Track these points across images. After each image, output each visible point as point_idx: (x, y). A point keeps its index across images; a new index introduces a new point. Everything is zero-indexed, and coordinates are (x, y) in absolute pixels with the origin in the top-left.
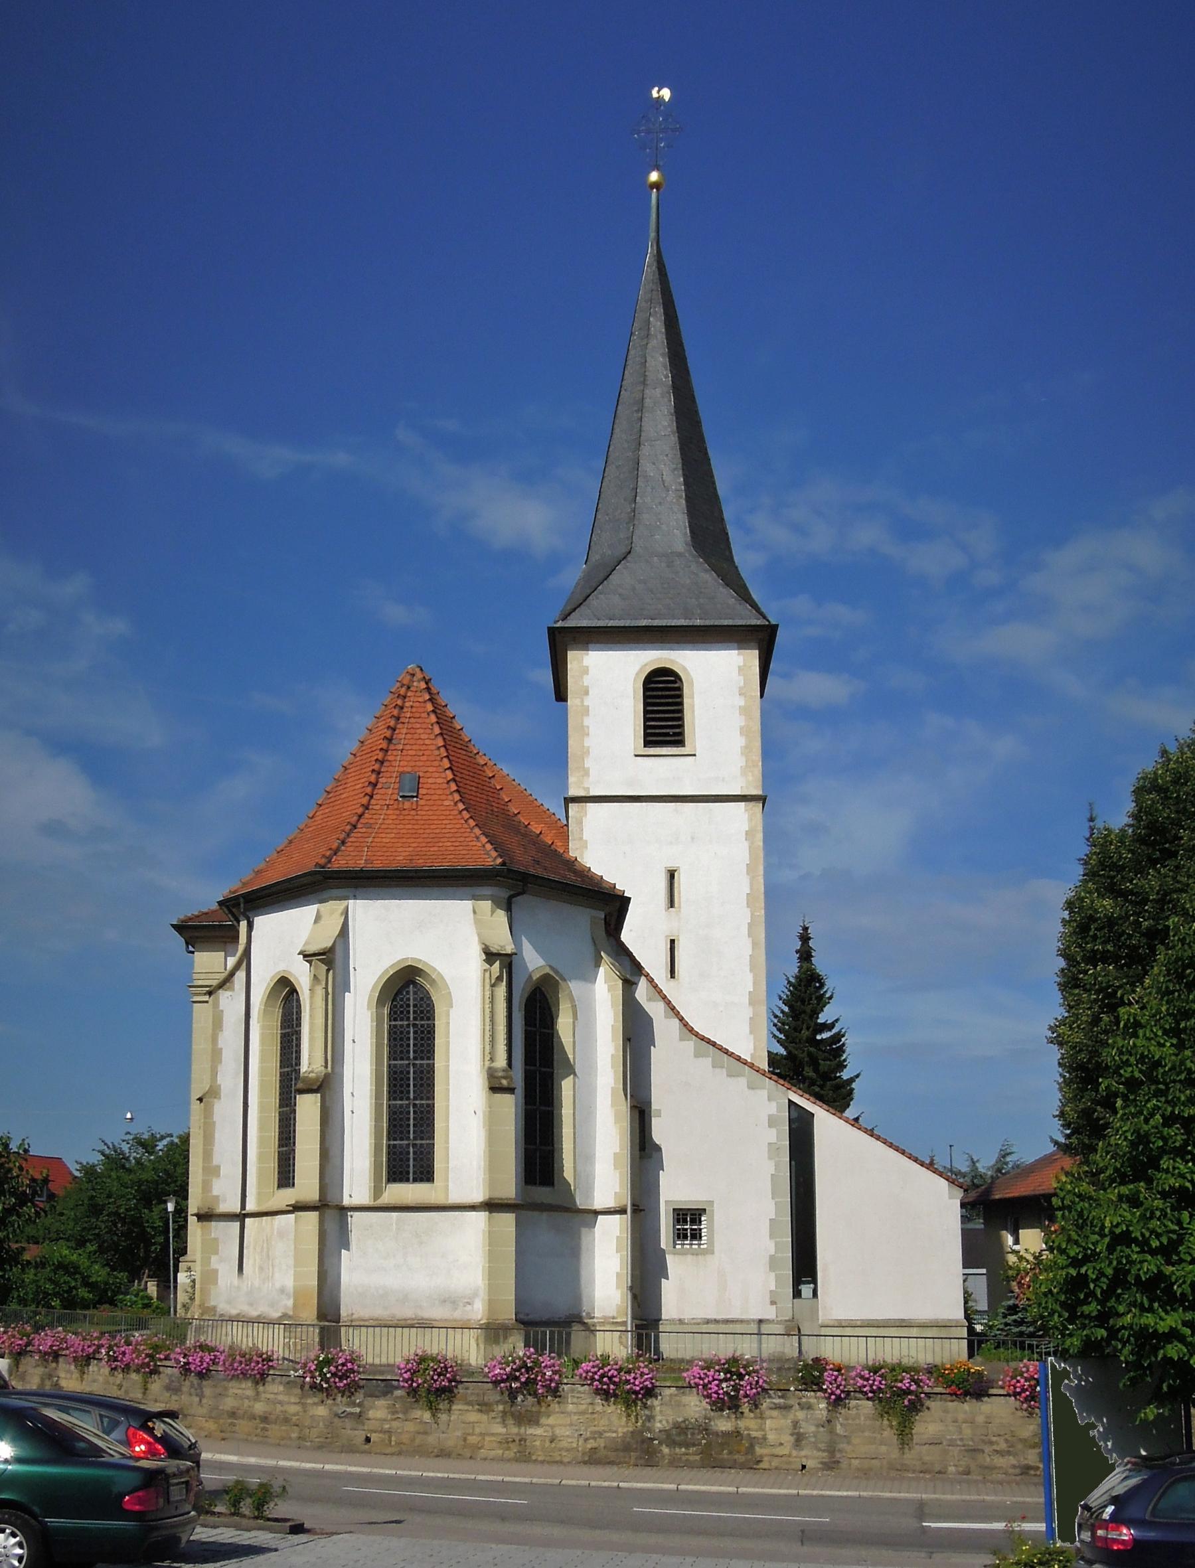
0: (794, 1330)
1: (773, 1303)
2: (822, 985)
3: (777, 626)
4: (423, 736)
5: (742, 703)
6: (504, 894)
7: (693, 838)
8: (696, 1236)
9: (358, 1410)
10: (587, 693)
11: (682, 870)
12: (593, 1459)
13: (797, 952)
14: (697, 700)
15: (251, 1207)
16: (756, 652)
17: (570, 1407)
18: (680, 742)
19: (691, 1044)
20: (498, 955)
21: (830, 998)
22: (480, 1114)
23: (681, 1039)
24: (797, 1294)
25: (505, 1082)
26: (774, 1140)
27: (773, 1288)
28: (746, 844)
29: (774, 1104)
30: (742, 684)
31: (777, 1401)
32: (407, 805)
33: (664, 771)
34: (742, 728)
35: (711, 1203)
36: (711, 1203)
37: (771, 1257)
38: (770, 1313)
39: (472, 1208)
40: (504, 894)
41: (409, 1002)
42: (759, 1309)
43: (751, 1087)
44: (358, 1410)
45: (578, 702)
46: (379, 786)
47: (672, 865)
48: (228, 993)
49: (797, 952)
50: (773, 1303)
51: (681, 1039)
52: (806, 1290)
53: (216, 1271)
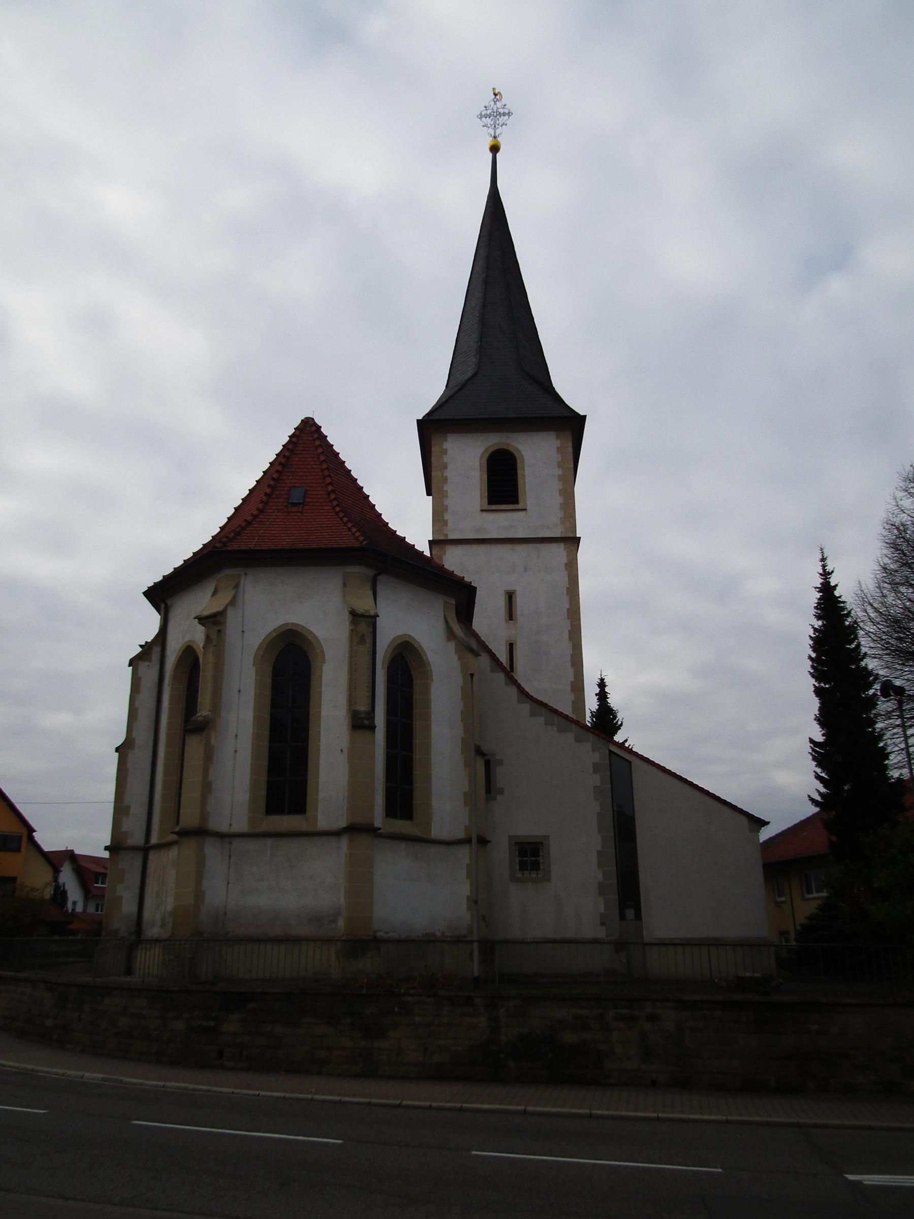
0: (620, 945)
1: (603, 924)
2: (615, 717)
3: (585, 416)
4: (312, 463)
5: (561, 473)
6: (371, 573)
7: (525, 570)
8: (536, 866)
9: (212, 1024)
10: (445, 467)
11: (518, 593)
12: (439, 1074)
13: (596, 695)
14: (527, 471)
15: (154, 840)
16: (570, 438)
17: (417, 1019)
18: (516, 502)
19: (527, 706)
20: (362, 616)
21: (621, 725)
22: (346, 751)
23: (519, 702)
24: (622, 917)
25: (366, 722)
26: (598, 784)
27: (602, 911)
28: (566, 573)
29: (597, 755)
30: (560, 459)
31: (623, 1011)
32: (294, 509)
33: (501, 523)
34: (560, 491)
35: (547, 837)
36: (547, 837)
37: (600, 884)
38: (601, 933)
39: (338, 833)
40: (371, 573)
41: (290, 662)
42: (591, 929)
43: (578, 740)
44: (212, 1024)
45: (439, 473)
46: (274, 496)
47: (510, 588)
48: (147, 663)
49: (596, 695)
50: (603, 924)
51: (519, 702)
52: (630, 913)
53: (121, 898)
